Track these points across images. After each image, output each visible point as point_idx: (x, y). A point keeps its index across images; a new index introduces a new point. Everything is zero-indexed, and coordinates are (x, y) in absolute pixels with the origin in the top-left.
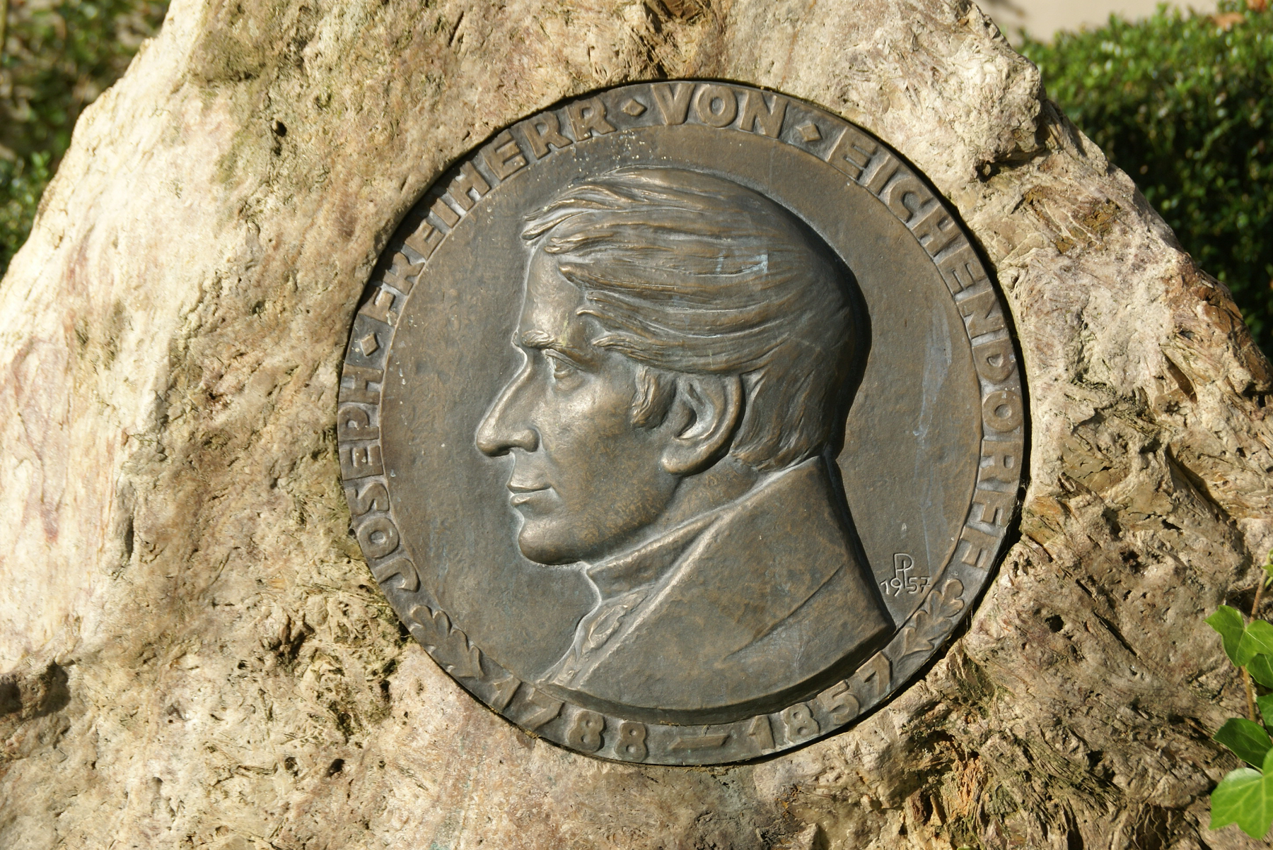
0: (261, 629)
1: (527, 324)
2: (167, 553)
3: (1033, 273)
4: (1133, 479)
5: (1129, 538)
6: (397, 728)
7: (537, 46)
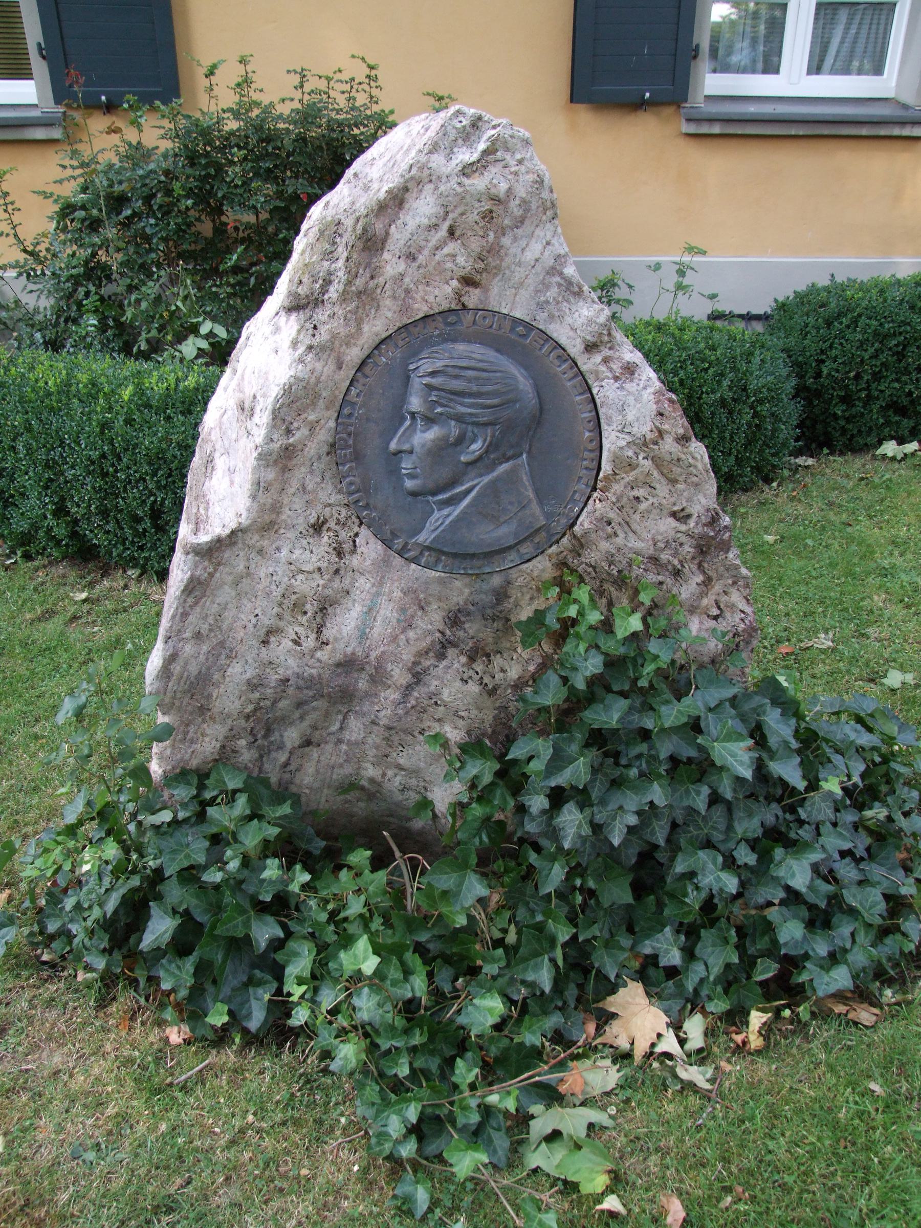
1: (409, 403)
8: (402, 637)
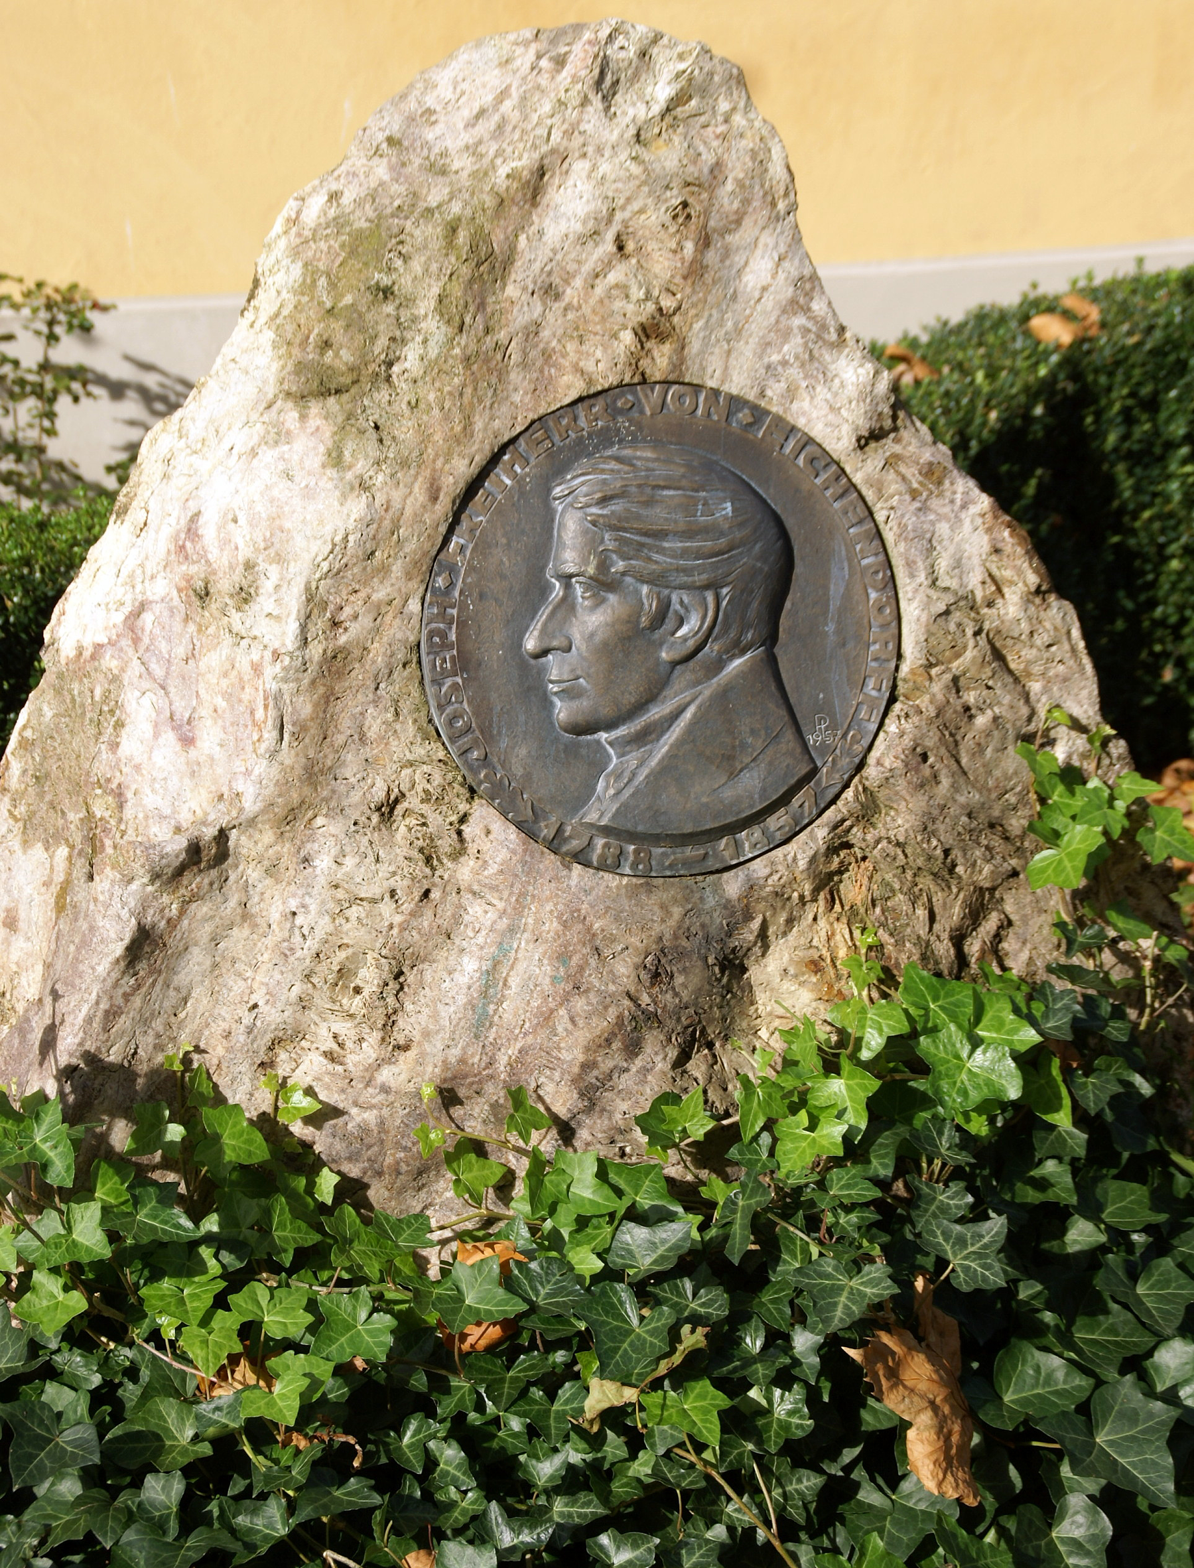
0: (368, 796)
2: (307, 740)
3: (899, 513)
4: (969, 654)
5: (965, 697)
6: (471, 863)
7: (561, 360)
8: (562, 1012)
